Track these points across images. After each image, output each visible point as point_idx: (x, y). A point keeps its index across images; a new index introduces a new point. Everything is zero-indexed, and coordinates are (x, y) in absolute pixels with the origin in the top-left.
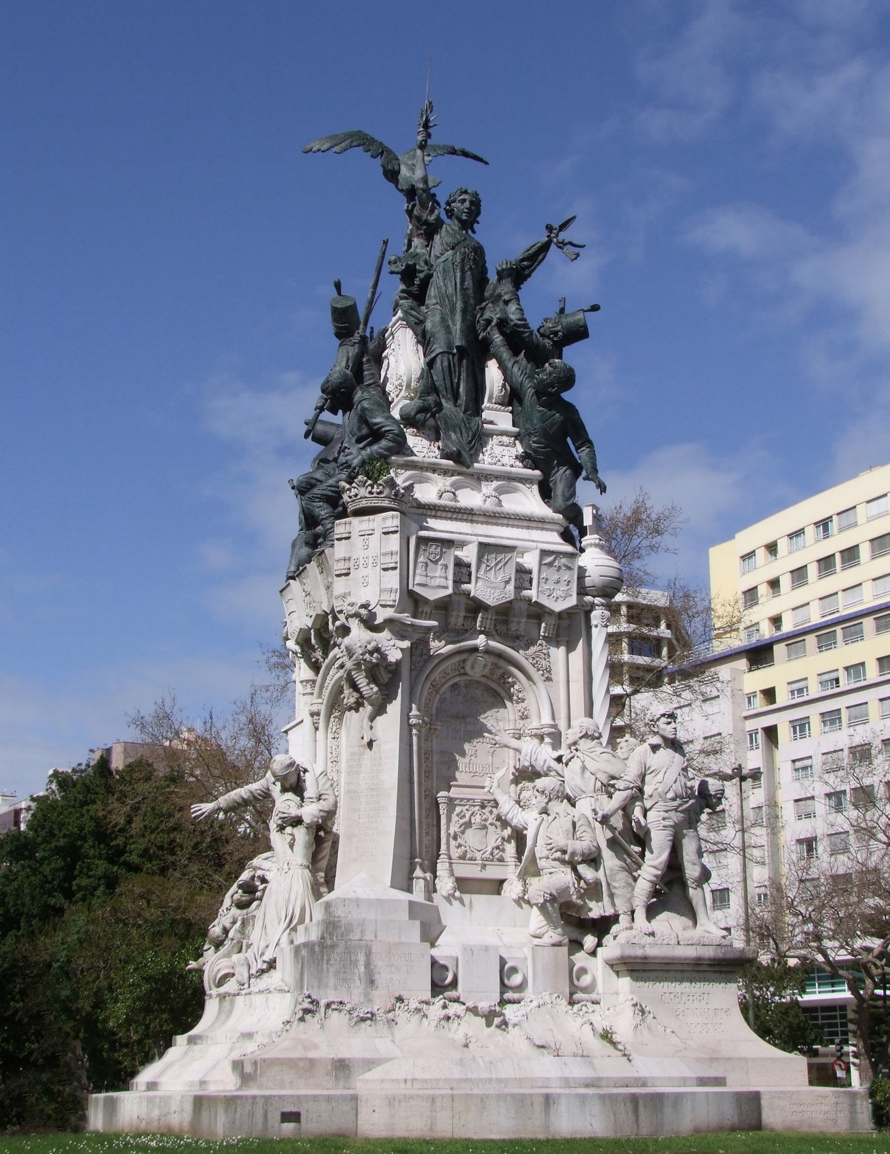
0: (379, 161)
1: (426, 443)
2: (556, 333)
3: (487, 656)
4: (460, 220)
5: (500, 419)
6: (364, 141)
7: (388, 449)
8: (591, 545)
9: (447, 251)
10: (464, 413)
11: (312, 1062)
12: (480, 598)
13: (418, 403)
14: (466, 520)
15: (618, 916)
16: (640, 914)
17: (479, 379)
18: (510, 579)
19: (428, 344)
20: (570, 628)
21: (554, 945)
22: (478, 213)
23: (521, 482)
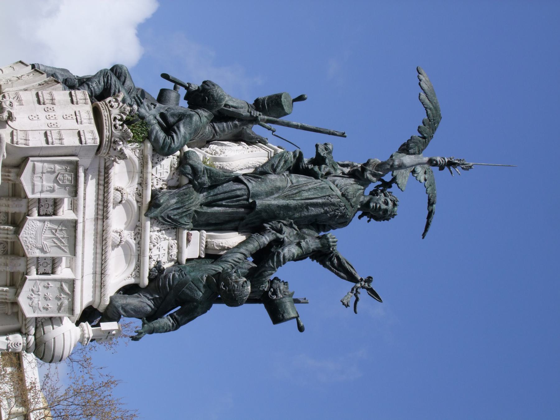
0: (417, 134)
1: (166, 176)
2: (275, 293)
4: (369, 202)
5: (194, 245)
6: (432, 122)
7: (156, 140)
8: (83, 331)
9: (340, 190)
10: (196, 211)
12: (26, 225)
13: (201, 167)
14: (97, 214)
17: (227, 226)
22: (377, 219)
23: (136, 268)
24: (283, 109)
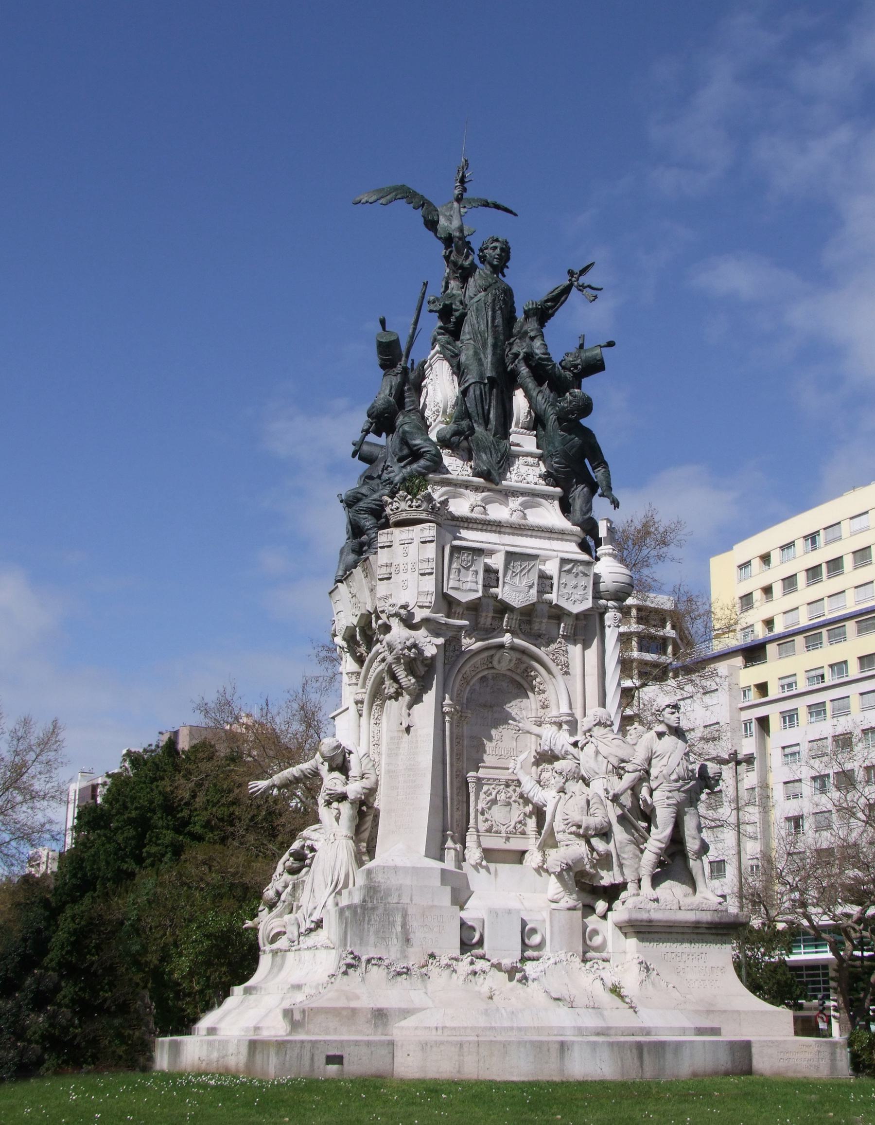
0: (420, 212)
1: (460, 462)
2: (576, 366)
3: (512, 652)
5: (525, 441)
8: (605, 554)
9: (480, 292)
11: (354, 1011)
13: (453, 427)
14: (495, 532)
15: (627, 883)
16: (646, 882)
17: (508, 407)
18: (533, 584)
19: (463, 375)
20: (585, 628)
21: (569, 909)
22: (508, 259)
23: (544, 498)
24: (394, 341)
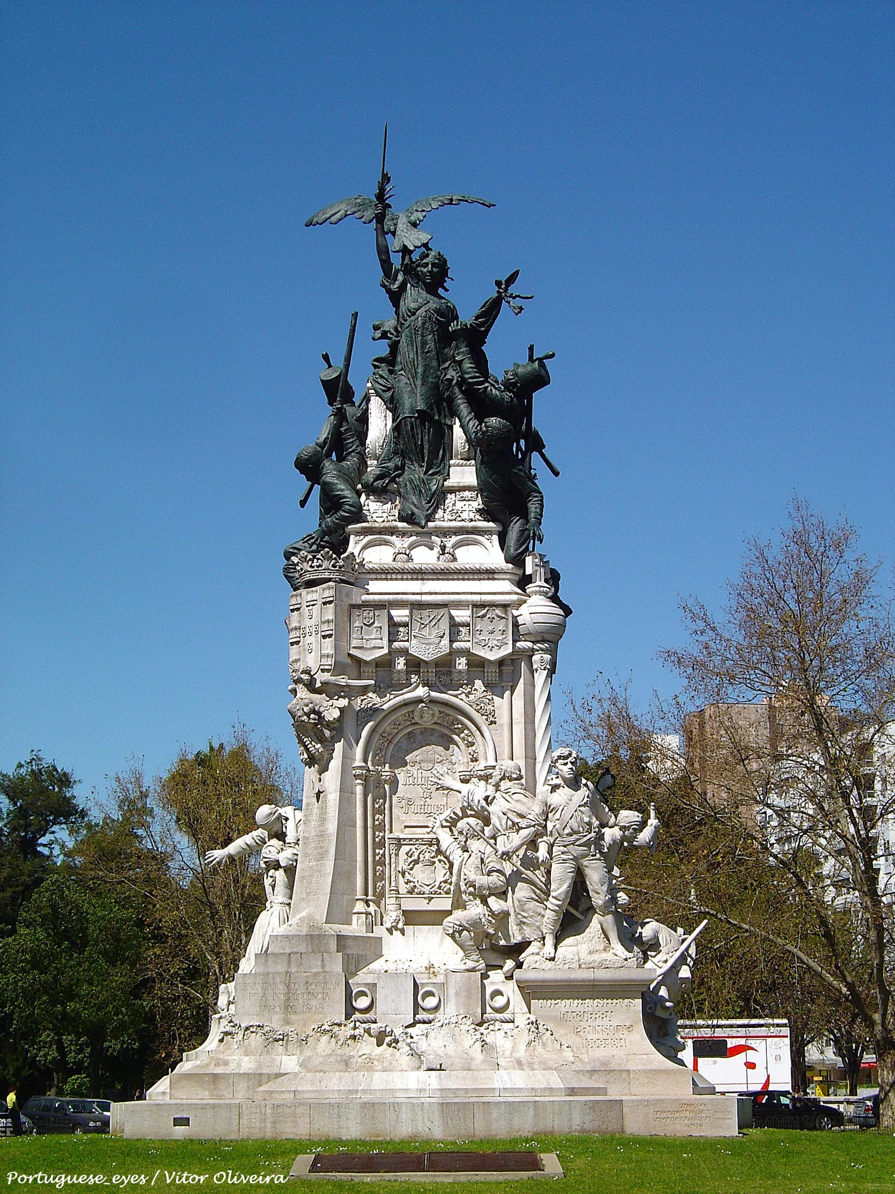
8: (536, 593)
16: (550, 941)
20: (502, 675)
21: (468, 970)
